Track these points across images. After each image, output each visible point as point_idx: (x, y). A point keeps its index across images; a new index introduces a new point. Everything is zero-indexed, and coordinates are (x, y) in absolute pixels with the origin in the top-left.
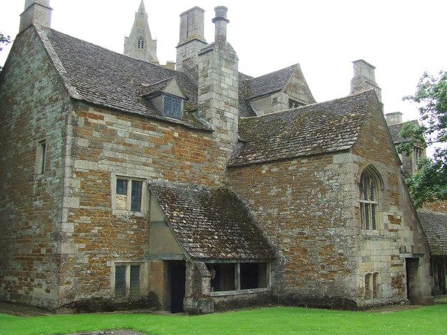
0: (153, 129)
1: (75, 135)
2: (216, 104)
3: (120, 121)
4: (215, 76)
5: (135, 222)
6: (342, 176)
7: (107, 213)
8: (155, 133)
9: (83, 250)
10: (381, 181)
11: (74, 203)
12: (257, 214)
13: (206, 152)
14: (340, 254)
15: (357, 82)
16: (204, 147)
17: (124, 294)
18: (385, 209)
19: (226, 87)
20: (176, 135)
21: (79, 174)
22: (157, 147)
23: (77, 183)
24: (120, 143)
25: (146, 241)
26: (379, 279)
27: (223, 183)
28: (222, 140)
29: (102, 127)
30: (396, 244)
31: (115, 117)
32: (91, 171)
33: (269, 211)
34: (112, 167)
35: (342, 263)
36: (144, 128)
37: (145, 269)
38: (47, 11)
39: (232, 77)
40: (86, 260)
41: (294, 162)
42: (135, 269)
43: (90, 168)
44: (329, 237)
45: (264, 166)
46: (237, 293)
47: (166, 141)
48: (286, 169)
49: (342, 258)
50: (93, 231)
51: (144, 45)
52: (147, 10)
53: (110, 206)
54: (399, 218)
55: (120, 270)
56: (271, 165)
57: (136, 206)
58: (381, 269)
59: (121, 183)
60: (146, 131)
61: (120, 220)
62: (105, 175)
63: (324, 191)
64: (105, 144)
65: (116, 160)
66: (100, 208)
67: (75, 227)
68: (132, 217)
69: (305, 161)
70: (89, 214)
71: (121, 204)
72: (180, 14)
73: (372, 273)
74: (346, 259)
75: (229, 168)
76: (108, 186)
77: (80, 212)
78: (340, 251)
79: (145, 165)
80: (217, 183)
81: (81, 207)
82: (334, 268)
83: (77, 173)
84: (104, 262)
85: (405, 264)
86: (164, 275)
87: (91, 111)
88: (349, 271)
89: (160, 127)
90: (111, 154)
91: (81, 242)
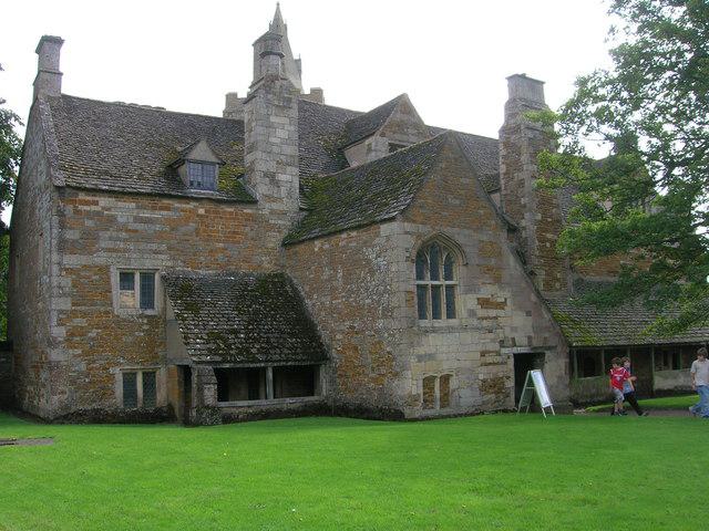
1: (62, 226)
2: (261, 167)
4: (260, 130)
5: (145, 321)
6: (389, 253)
7: (107, 313)
8: (170, 213)
10: (462, 252)
11: (65, 304)
12: (315, 304)
13: (248, 229)
15: (513, 107)
17: (135, 405)
18: (470, 289)
20: (201, 211)
21: (70, 271)
23: (67, 282)
26: (453, 383)
28: (272, 212)
30: (492, 336)
33: (323, 299)
35: (390, 366)
36: (154, 208)
41: (344, 235)
42: (149, 378)
46: (268, 402)
47: (187, 220)
49: (391, 358)
52: (285, 17)
54: (499, 300)
55: (129, 380)
56: (322, 241)
57: (147, 300)
58: (458, 371)
59: (126, 278)
61: (124, 320)
62: (104, 270)
63: (372, 272)
68: (141, 316)
69: (354, 234)
70: (84, 315)
71: (127, 302)
72: (253, 42)
75: (284, 245)
77: (72, 314)
79: (156, 252)
82: (383, 371)
83: (66, 270)
85: (511, 362)
86: (179, 382)
87: (82, 196)
90: (110, 245)
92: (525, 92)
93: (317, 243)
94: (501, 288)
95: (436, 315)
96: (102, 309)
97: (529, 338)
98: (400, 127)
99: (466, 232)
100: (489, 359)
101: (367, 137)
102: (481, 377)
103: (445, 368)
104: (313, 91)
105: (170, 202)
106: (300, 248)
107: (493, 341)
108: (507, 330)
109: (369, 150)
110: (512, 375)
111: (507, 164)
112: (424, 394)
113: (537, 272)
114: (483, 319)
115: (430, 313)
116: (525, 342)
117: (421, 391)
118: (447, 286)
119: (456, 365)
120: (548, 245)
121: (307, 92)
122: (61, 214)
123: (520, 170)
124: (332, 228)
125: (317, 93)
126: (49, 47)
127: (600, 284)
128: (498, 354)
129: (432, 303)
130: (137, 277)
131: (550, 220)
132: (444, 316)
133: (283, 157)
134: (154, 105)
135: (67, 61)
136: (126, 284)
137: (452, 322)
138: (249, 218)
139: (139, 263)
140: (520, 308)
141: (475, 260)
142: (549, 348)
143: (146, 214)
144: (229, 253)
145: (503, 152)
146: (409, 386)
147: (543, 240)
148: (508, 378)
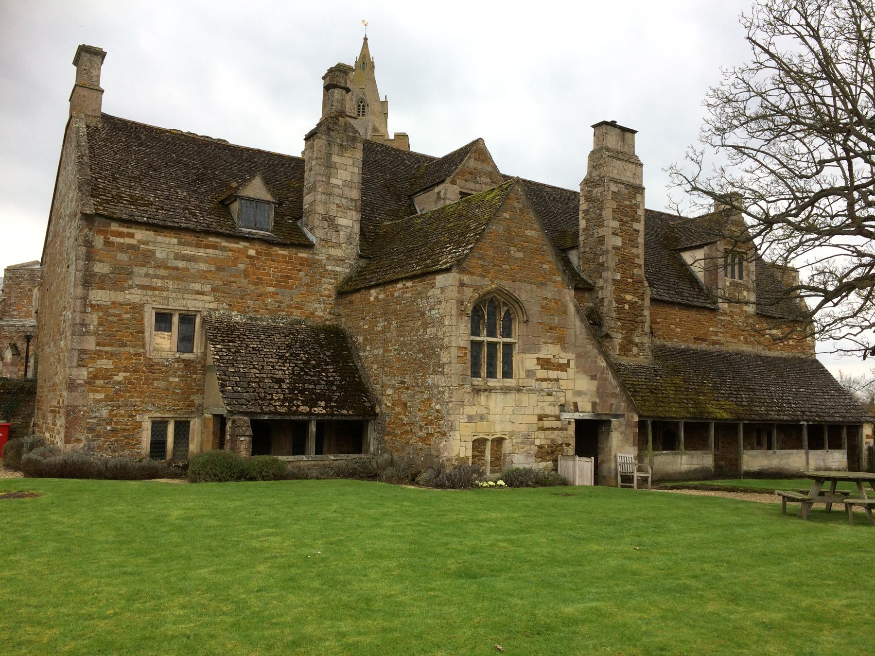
0: (214, 247)
1: (90, 257)
3: (160, 239)
7: (138, 355)
8: (217, 252)
9: (101, 400)
13: (302, 274)
14: (438, 411)
15: (596, 159)
16: (299, 267)
19: (339, 182)
20: (252, 252)
22: (219, 269)
24: (159, 267)
25: (198, 390)
26: (507, 447)
27: (330, 313)
29: (132, 247)
30: (551, 399)
31: (152, 233)
32: (114, 303)
33: (376, 352)
34: (146, 297)
35: (439, 426)
36: (198, 246)
37: (195, 424)
38: (95, 94)
39: (350, 169)
40: (105, 413)
41: (400, 285)
43: (112, 300)
44: (429, 388)
45: (372, 291)
48: (392, 295)
50: (115, 378)
51: (366, 111)
53: (143, 346)
54: (562, 361)
55: (158, 427)
56: (378, 290)
57: (185, 341)
58: (512, 435)
60: (202, 250)
61: (158, 364)
62: (137, 309)
64: (136, 269)
65: (154, 289)
66: (127, 349)
67: (89, 373)
68: (178, 360)
69: (409, 284)
70: (110, 356)
71: (164, 344)
73: (490, 438)
74: (442, 418)
76: (141, 321)
78: (438, 407)
80: (321, 314)
81: (98, 348)
82: (431, 430)
83: (92, 306)
84: (132, 416)
85: (573, 427)
86: (214, 432)
87: (115, 227)
88: (444, 435)
89: (224, 244)
90: (146, 281)
91: (98, 392)
92: (614, 142)
93: (373, 292)
94: (564, 349)
95: (491, 374)
96: (131, 350)
97: (594, 404)
98: (474, 174)
99: (529, 287)
100: (547, 424)
101: (438, 184)
102: (538, 442)
103: (498, 430)
104: (397, 136)
105: (218, 240)
106: (356, 297)
107: (552, 404)
108: (569, 394)
109: (439, 197)
110: (573, 442)
111: (587, 219)
112: (474, 457)
113: (614, 335)
114: (543, 380)
115: (484, 372)
116: (589, 408)
117: (470, 453)
118: (505, 344)
119: (509, 428)
120: (627, 307)
121: (392, 137)
122: (88, 244)
123: (601, 225)
124: (390, 277)
125: (402, 137)
126: (89, 58)
127: (684, 352)
128: (558, 418)
129: (487, 362)
130: (176, 319)
131: (630, 280)
132: (500, 374)
133: (344, 201)
134: (215, 135)
135: (109, 76)
136: (163, 325)
137: (510, 382)
138: (303, 262)
139: (178, 303)
140: (585, 372)
141: (534, 319)
142: (616, 416)
143: (189, 251)
144: (280, 297)
145: (583, 206)
146: (457, 448)
147: (620, 301)
148: (568, 445)
